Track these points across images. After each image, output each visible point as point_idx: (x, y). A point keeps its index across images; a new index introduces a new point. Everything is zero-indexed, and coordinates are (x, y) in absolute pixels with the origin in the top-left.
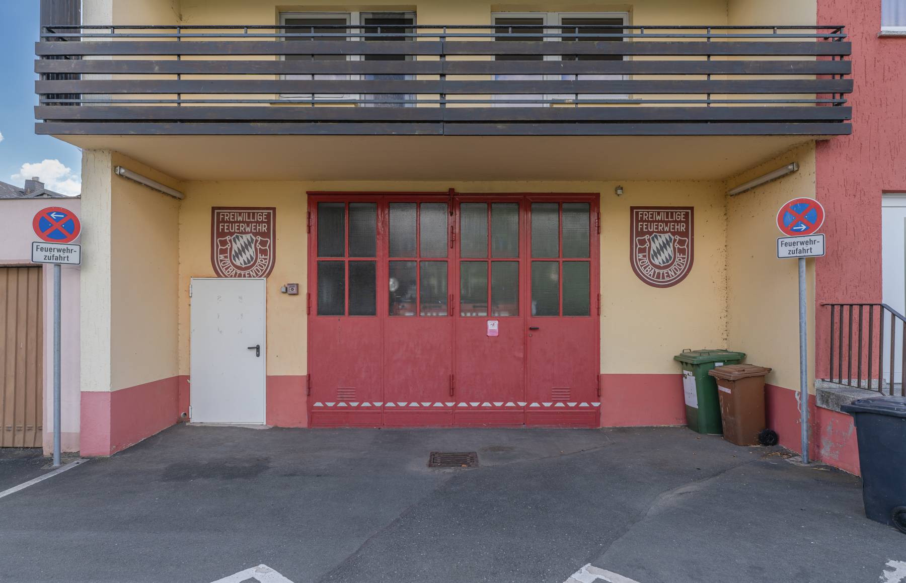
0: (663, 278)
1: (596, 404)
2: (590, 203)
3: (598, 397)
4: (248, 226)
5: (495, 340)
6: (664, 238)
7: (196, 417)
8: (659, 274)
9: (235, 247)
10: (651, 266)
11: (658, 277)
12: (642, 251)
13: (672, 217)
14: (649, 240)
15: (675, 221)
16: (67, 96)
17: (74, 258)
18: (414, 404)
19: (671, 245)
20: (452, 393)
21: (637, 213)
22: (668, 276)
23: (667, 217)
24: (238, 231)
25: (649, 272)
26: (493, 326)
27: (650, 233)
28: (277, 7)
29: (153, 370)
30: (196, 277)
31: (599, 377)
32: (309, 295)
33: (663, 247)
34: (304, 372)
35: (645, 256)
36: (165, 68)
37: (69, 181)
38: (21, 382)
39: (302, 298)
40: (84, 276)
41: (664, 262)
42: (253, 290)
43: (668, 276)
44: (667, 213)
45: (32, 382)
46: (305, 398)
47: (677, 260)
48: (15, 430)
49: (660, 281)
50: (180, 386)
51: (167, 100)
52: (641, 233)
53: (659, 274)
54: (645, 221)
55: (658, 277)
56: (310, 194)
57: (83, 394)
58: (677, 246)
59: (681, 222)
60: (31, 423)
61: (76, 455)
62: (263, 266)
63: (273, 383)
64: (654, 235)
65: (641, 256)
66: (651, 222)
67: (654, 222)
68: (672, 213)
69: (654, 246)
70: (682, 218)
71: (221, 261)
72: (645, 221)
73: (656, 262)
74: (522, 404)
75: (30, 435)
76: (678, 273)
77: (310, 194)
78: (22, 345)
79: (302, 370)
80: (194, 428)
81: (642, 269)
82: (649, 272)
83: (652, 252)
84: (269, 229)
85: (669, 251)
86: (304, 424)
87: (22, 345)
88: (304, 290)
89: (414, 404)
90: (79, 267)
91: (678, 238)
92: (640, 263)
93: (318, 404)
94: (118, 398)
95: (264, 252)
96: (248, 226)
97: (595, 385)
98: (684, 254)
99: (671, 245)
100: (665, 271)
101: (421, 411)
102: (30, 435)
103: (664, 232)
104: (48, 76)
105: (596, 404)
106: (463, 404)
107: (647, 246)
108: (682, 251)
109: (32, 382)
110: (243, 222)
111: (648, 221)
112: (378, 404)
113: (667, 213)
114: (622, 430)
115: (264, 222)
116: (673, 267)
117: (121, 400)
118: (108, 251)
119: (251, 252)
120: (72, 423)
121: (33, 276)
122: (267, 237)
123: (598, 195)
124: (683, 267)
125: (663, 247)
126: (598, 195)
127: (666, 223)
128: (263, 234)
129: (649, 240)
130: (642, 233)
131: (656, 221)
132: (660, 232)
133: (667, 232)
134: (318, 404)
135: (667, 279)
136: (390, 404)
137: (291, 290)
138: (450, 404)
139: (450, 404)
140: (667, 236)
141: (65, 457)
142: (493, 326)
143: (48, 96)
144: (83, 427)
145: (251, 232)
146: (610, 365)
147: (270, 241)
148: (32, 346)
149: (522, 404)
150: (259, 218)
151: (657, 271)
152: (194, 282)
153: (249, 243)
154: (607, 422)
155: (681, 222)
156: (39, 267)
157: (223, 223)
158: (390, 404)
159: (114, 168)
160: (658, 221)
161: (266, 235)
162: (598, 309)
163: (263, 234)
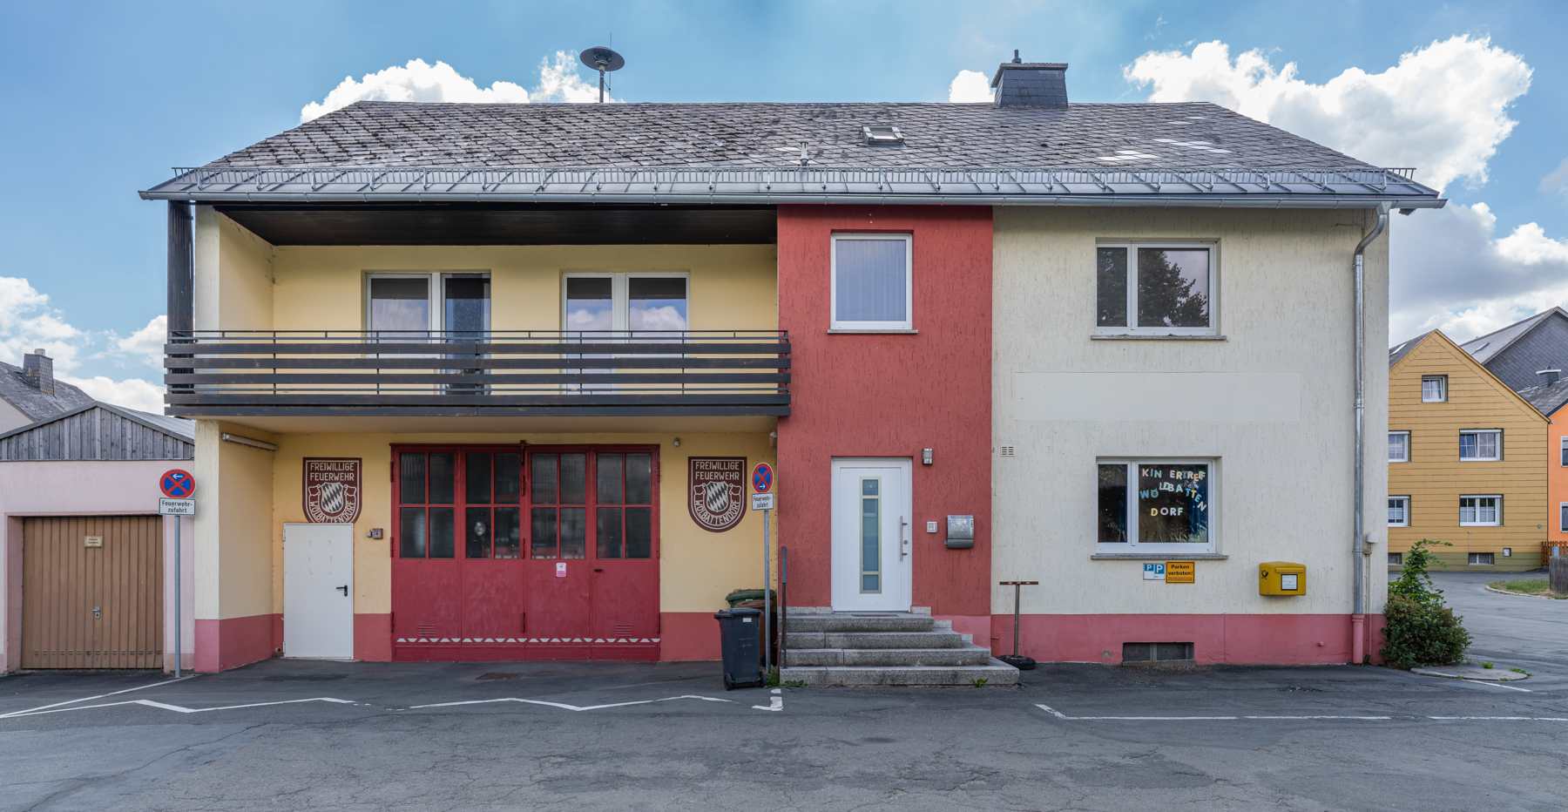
1: (656, 640)
2: (651, 451)
3: (658, 634)
5: (563, 581)
6: (719, 485)
7: (290, 651)
9: (325, 495)
12: (699, 498)
16: (186, 386)
17: (190, 510)
18: (489, 640)
20: (524, 631)
24: (325, 481)
25: (706, 517)
26: (561, 568)
28: (365, 274)
29: (252, 607)
30: (289, 522)
31: (659, 615)
32: (392, 540)
33: (719, 494)
34: (389, 611)
36: (264, 363)
37: (44, 319)
38: (143, 614)
39: (385, 544)
40: (197, 524)
42: (341, 534)
45: (151, 613)
46: (389, 635)
48: (138, 653)
49: (715, 526)
50: (274, 624)
51: (266, 389)
52: (698, 482)
56: (393, 446)
57: (197, 622)
60: (151, 648)
61: (192, 671)
62: (350, 511)
63: (361, 621)
69: (710, 494)
74: (588, 640)
75: (150, 658)
77: (393, 446)
78: (143, 582)
79: (385, 608)
80: (287, 660)
85: (724, 498)
86: (389, 659)
87: (143, 582)
88: (388, 534)
89: (489, 640)
90: (192, 518)
93: (401, 640)
94: (224, 624)
95: (351, 499)
97: (656, 622)
101: (496, 646)
102: (150, 658)
104: (176, 371)
105: (656, 640)
106: (534, 640)
109: (151, 613)
112: (456, 640)
114: (674, 663)
115: (350, 472)
117: (228, 628)
118: (217, 504)
119: (339, 499)
120: (188, 647)
121: (152, 523)
122: (353, 485)
123: (658, 446)
125: (719, 494)
126: (658, 446)
128: (350, 483)
134: (401, 640)
136: (467, 640)
137: (376, 534)
138: (522, 640)
139: (522, 640)
141: (183, 672)
142: (561, 568)
143: (174, 386)
144: (197, 649)
146: (667, 606)
147: (357, 489)
148: (151, 583)
149: (588, 640)
150: (346, 468)
152: (287, 528)
154: (666, 657)
156: (157, 517)
157: (313, 474)
158: (467, 640)
159: (221, 435)
161: (353, 483)
162: (658, 552)
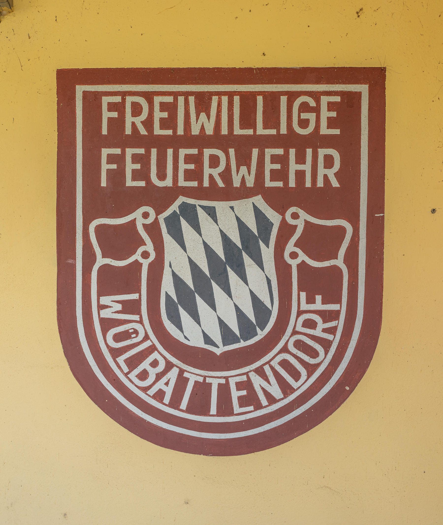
0: (225, 407)
4: (244, 160)
6: (228, 219)
8: (202, 389)
9: (178, 261)
10: (161, 355)
11: (200, 404)
12: (117, 281)
13: (271, 120)
14: (153, 230)
15: (290, 140)
19: (267, 253)
21: (92, 100)
22: (250, 399)
23: (248, 120)
27: (159, 199)
33: (228, 262)
35: (131, 307)
41: (227, 335)
43: (250, 399)
44: (248, 101)
47: (295, 322)
49: (208, 422)
53: (202, 389)
54: (136, 139)
55: (200, 404)
58: (297, 258)
59: (316, 140)
64: (174, 209)
65: (112, 305)
66: (162, 144)
67: (177, 142)
68: (272, 100)
70: (323, 121)
71: (107, 324)
72: (136, 139)
73: (191, 334)
76: (301, 385)
81: (119, 366)
82: (156, 380)
83: (167, 286)
84: (349, 173)
85: (257, 280)
91: (301, 219)
92: (107, 341)
96: (244, 160)
98: (332, 297)
99: (267, 253)
100: (235, 376)
103: (230, 193)
107: (142, 257)
108: (322, 284)
110: (218, 140)
111: (150, 141)
113: (248, 101)
116: (273, 358)
124: (324, 359)
125: (228, 262)
127: (243, 148)
128: (317, 200)
129: (153, 230)
130: (118, 199)
131: (188, 140)
132: (212, 193)
133: (244, 193)
135: (241, 413)
140: (245, 209)
145: (260, 188)
147: (353, 231)
151: (194, 375)
153: (251, 243)
155: (316, 140)
160: (202, 141)
163: (317, 200)
